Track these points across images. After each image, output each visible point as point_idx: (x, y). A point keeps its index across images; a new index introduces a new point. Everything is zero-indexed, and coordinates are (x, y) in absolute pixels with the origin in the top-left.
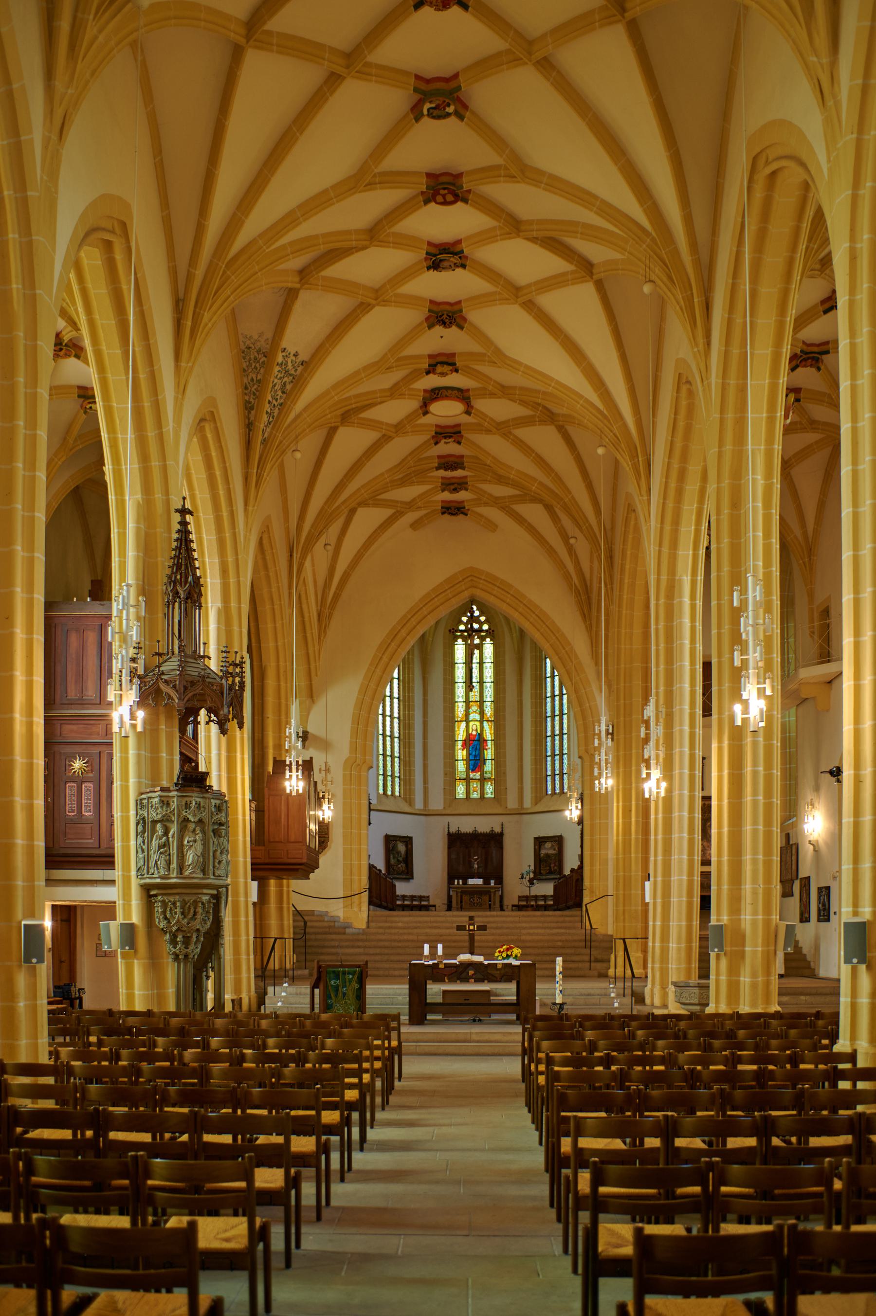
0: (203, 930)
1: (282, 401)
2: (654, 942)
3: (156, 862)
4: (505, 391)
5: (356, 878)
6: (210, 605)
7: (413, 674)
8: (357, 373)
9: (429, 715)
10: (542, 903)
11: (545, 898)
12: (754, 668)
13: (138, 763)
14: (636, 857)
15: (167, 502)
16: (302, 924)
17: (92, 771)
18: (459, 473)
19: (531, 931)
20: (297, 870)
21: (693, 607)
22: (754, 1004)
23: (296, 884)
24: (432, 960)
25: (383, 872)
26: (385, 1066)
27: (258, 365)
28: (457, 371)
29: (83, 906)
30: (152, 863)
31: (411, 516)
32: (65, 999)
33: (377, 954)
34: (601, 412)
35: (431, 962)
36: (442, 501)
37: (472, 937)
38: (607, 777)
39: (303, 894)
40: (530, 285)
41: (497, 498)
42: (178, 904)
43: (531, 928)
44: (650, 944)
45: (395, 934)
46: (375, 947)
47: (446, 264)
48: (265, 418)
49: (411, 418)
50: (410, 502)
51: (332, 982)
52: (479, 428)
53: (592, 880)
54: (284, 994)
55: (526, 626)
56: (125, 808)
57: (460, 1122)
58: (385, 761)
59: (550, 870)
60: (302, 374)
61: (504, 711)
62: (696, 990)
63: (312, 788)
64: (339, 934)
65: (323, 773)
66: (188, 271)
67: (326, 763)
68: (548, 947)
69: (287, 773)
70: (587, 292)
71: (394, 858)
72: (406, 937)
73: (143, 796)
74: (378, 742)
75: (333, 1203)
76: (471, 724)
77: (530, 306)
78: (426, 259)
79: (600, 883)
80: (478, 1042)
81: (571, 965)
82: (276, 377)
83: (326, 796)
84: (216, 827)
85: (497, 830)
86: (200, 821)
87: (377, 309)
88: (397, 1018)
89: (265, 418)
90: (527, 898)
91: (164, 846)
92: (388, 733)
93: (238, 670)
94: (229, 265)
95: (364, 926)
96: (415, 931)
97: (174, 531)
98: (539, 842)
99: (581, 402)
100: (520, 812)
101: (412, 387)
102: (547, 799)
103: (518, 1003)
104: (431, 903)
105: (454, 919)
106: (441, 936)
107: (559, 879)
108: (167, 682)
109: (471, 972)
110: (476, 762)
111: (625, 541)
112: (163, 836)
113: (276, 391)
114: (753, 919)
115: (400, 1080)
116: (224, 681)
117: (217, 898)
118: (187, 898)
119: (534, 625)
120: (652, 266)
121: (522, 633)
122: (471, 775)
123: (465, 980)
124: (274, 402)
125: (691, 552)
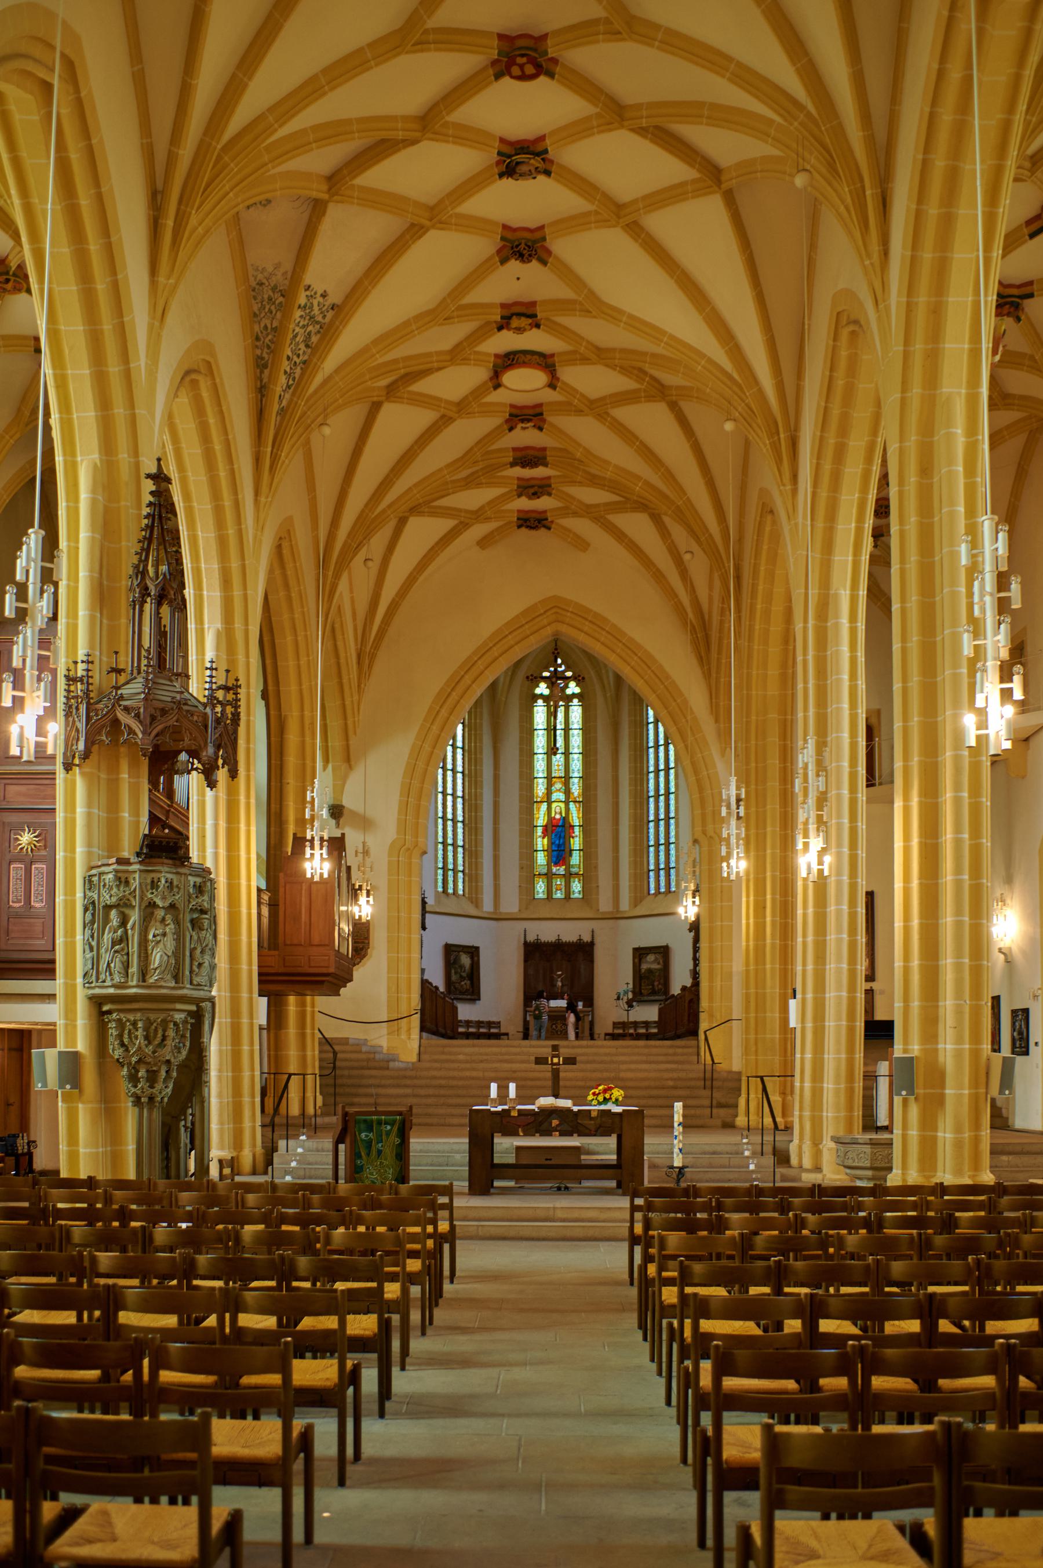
0: (175, 1062)
1: (306, 357)
2: (802, 1081)
3: (109, 965)
4: (601, 355)
5: (404, 996)
6: (206, 626)
7: (481, 719)
8: (406, 324)
9: (501, 794)
10: (642, 1031)
11: (647, 1024)
12: (995, 659)
13: (89, 826)
14: (773, 969)
15: (137, 465)
16: (331, 1055)
17: (45, 847)
18: (540, 472)
19: (633, 1066)
20: (322, 982)
21: (853, 631)
22: (958, 1172)
23: (323, 1002)
24: (500, 1105)
25: (442, 989)
26: (427, 1269)
27: (273, 308)
28: (538, 326)
29: (40, 1031)
30: (103, 966)
31: (479, 530)
32: (7, 1155)
33: (429, 1096)
34: (730, 377)
35: (500, 1108)
36: (519, 511)
37: (556, 1074)
38: (738, 858)
39: (330, 1014)
40: (635, 201)
41: (589, 506)
42: (140, 1024)
43: (632, 1062)
44: (797, 1084)
45: (454, 1069)
46: (428, 1086)
47: (524, 168)
48: (283, 380)
49: (477, 393)
50: (477, 511)
51: (363, 1135)
52: (568, 408)
53: (711, 999)
54: (300, 1150)
55: (626, 672)
56: (70, 889)
57: (539, 1365)
58: (445, 851)
59: (653, 989)
60: (332, 322)
61: (596, 789)
62: (867, 1149)
63: (344, 875)
64: (381, 1068)
65: (360, 856)
66: (170, 151)
67: (364, 843)
68: (656, 1088)
69: (308, 851)
70: (713, 206)
71: (456, 973)
72: (468, 1074)
73: (94, 872)
74: (436, 827)
75: (319, 1538)
76: (554, 805)
77: (636, 230)
78: (498, 163)
79: (724, 1002)
80: (564, 1220)
81: (692, 1112)
82: (298, 325)
83: (364, 887)
84: (195, 916)
85: (587, 938)
86: (172, 906)
87: (432, 234)
88: (448, 1191)
89: (283, 380)
90: (624, 1025)
91: (121, 941)
92: (450, 816)
93: (230, 696)
94: (225, 149)
95: (414, 1058)
96: (482, 1065)
97: (144, 505)
98: (640, 953)
99: (703, 362)
100: (616, 916)
101: (477, 349)
102: (651, 895)
103: (618, 1166)
104: (503, 1031)
105: (532, 1050)
106: (515, 1072)
107: (666, 1000)
108: (127, 709)
109: (555, 1122)
110: (559, 853)
111: (757, 554)
112: (120, 927)
113: (298, 344)
114: (956, 1050)
115: (452, 1282)
116: (208, 710)
117: (197, 1017)
118: (152, 1016)
119: (635, 670)
120: (807, 155)
121: (619, 680)
122: (554, 869)
123: (547, 1133)
124: (295, 358)
125: (850, 558)
